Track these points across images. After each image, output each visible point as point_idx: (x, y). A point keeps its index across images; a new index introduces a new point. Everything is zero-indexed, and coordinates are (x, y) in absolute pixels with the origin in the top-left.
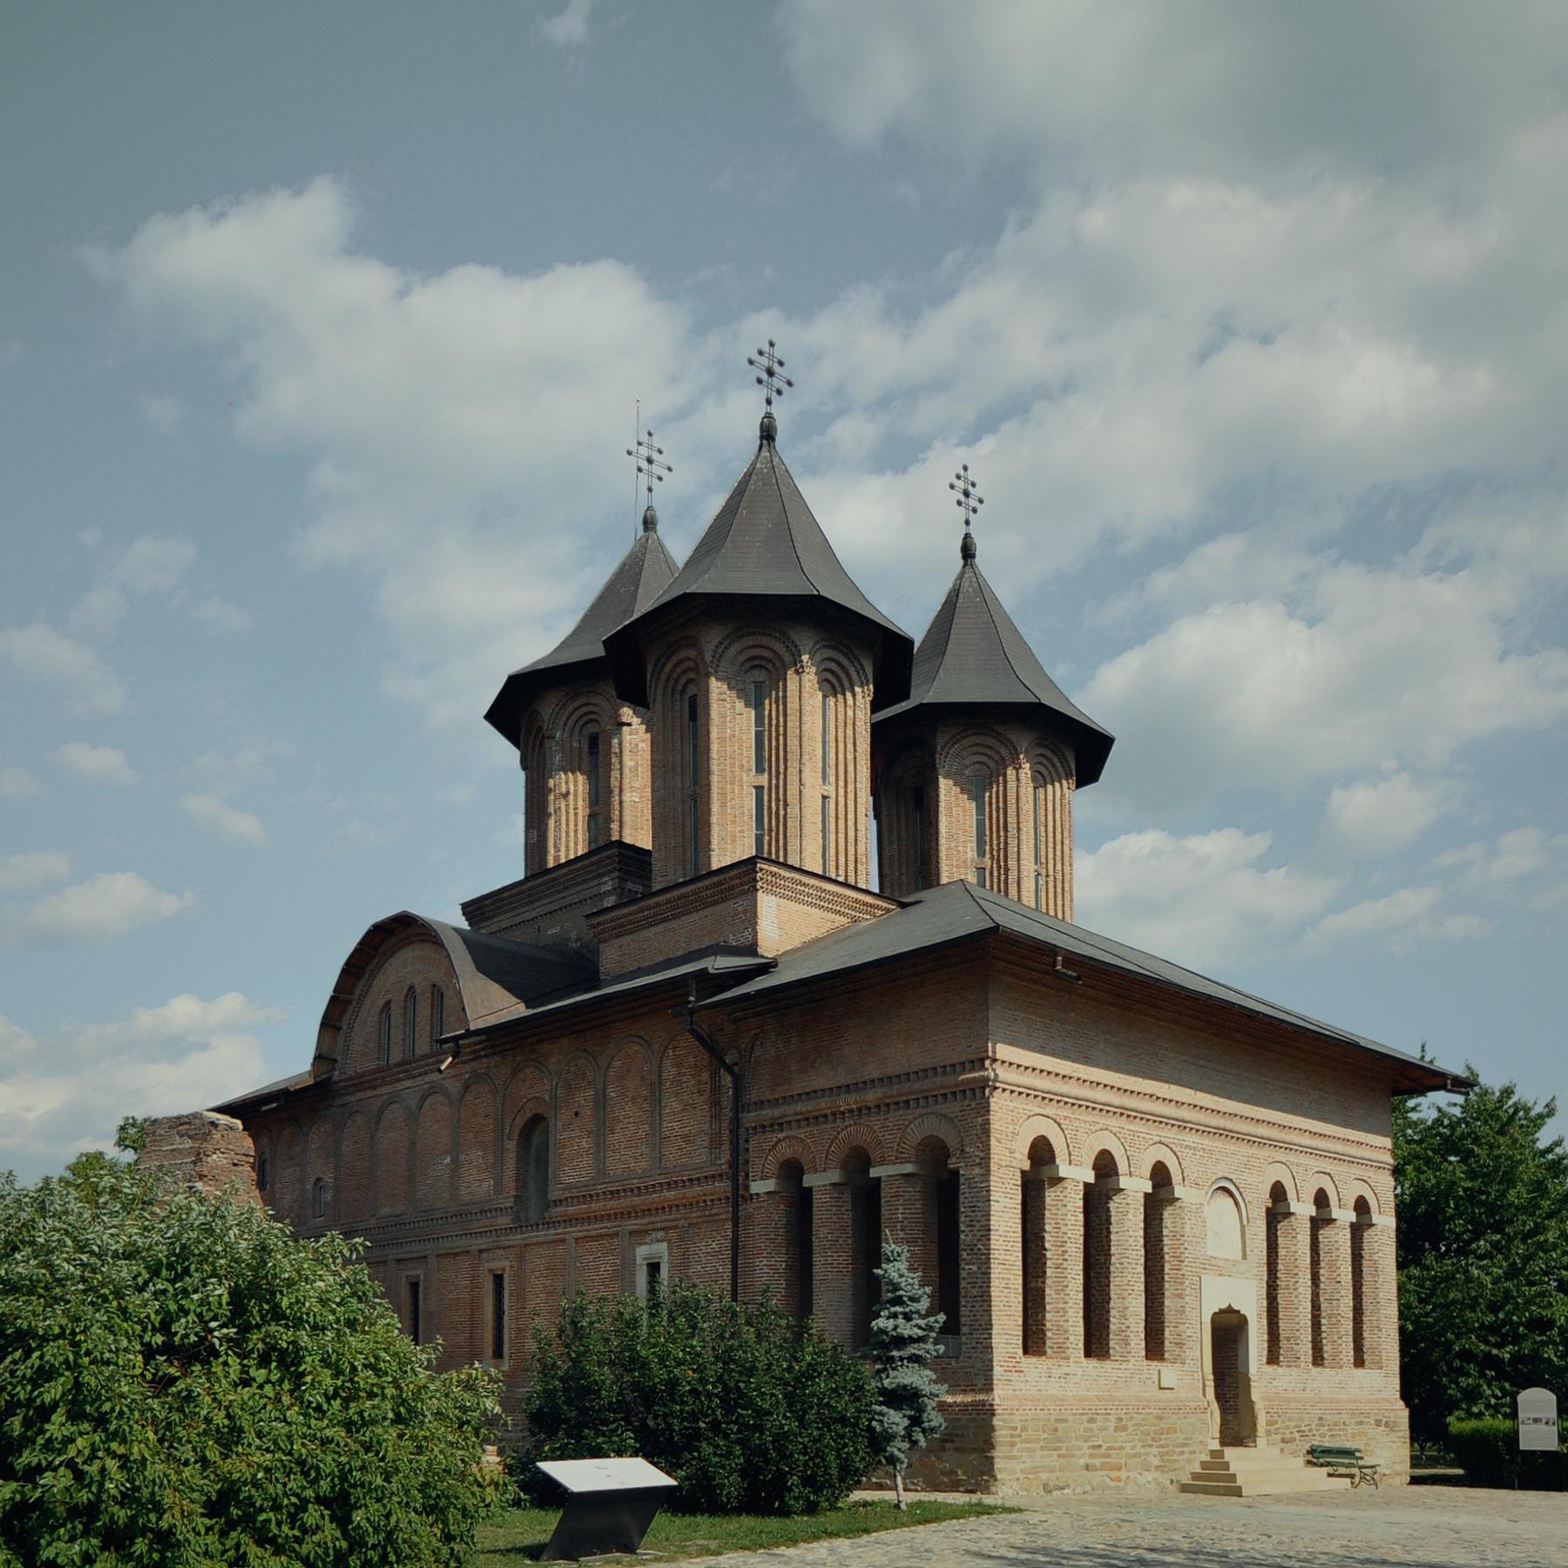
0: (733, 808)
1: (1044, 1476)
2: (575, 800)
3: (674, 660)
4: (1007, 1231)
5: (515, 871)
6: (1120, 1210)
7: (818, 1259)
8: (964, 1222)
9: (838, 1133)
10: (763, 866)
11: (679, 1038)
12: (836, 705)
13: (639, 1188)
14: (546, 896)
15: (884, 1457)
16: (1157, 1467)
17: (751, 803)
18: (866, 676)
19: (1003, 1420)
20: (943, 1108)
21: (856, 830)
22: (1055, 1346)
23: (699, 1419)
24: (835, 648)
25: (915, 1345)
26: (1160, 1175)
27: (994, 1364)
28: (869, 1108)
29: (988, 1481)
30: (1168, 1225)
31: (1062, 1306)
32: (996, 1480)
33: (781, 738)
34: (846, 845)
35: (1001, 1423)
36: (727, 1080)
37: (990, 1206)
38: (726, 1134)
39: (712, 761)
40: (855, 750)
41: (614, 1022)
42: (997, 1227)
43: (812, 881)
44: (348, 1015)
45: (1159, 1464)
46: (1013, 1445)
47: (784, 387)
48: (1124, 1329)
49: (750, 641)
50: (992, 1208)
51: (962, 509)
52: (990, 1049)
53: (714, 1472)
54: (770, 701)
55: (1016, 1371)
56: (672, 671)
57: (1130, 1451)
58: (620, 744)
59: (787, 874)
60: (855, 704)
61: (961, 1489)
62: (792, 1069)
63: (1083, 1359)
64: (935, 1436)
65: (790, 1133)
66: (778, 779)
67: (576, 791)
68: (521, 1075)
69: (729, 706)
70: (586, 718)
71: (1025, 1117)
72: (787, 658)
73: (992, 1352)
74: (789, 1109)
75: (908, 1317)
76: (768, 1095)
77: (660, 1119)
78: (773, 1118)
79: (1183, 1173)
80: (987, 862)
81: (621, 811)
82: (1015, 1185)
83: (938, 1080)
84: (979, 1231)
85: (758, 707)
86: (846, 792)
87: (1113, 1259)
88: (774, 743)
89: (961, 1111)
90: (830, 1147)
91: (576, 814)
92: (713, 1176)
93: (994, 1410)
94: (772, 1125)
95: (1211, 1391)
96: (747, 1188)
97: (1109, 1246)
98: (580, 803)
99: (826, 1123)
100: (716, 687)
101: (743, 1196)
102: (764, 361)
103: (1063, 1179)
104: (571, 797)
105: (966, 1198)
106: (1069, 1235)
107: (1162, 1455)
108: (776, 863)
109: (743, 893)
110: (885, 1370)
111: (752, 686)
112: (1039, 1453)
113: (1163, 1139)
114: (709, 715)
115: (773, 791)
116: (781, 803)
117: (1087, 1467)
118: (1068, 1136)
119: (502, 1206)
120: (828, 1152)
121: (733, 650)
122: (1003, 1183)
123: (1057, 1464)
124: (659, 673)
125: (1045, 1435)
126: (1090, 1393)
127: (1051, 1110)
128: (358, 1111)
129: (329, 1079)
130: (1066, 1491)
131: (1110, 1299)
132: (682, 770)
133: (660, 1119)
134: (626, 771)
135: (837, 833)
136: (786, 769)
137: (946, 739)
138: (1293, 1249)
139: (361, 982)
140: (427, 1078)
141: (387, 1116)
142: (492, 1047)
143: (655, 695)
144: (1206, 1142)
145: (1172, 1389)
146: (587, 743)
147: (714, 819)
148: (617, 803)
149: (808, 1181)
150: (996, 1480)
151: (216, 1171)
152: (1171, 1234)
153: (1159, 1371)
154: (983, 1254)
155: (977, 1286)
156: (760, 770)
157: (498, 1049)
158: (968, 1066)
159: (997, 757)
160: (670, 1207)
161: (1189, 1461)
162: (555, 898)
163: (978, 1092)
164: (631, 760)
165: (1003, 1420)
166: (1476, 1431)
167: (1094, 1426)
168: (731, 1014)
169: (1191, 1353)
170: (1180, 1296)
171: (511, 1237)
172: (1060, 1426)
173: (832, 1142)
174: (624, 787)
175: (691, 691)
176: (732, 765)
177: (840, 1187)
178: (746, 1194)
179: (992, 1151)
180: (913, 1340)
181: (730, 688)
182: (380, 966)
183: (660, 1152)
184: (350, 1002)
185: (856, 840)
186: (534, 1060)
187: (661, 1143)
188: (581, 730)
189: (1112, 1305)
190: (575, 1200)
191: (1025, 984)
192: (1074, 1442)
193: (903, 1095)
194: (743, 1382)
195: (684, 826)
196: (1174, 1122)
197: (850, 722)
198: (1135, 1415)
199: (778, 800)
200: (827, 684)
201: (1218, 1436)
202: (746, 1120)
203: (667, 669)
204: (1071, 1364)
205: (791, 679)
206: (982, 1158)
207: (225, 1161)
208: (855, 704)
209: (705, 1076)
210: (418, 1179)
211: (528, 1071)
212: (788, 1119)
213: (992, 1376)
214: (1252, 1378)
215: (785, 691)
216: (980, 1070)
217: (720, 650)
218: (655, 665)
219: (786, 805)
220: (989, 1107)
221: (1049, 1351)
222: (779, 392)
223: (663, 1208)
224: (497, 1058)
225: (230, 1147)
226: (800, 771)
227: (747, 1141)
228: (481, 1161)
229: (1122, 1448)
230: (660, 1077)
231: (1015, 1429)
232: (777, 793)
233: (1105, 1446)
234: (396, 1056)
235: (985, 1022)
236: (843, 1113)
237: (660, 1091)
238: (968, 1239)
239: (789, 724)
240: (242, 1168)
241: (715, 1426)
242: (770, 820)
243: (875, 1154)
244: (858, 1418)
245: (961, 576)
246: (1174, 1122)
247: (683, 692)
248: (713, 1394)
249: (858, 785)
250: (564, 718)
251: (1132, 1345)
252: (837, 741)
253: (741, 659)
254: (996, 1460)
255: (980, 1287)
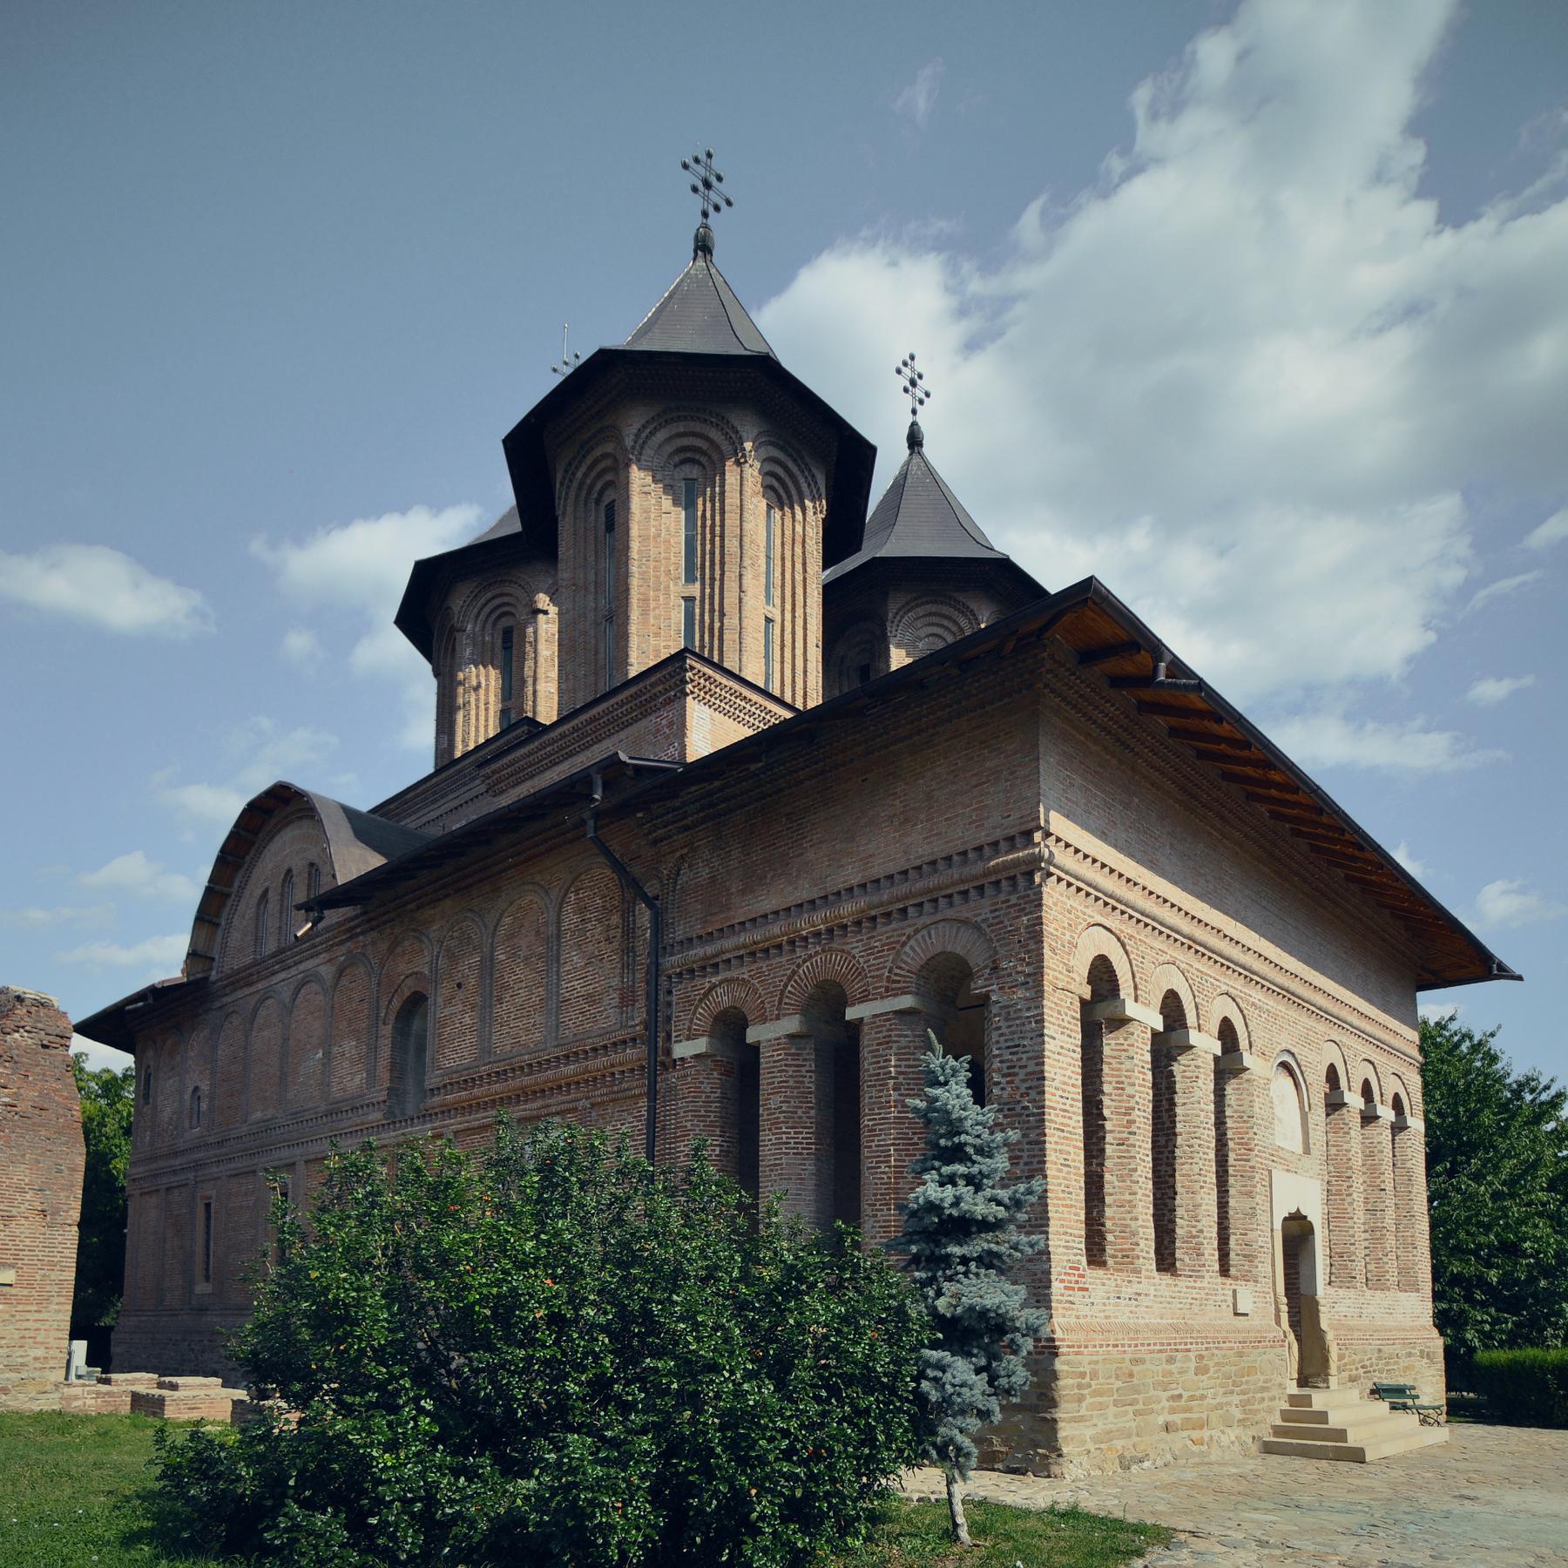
0: (657, 618)
1: (1119, 1444)
2: (487, 695)
3: (589, 460)
4: (1065, 1083)
5: (426, 766)
6: (1187, 1074)
7: (767, 1138)
8: (999, 1070)
9: (799, 966)
10: (694, 664)
11: (583, 877)
12: (783, 519)
13: (530, 1065)
14: (452, 791)
15: (934, 1445)
16: (1239, 1421)
17: (679, 616)
18: (818, 490)
19: (1068, 1363)
20: (961, 910)
21: (805, 660)
22: (1120, 1254)
23: (566, 1376)
24: (782, 449)
25: (990, 1236)
26: (1227, 1032)
27: (1053, 1277)
28: (845, 927)
29: (1047, 1457)
30: (1232, 1102)
31: (1128, 1197)
32: (1060, 1456)
33: (717, 539)
34: (794, 677)
35: (1065, 1368)
36: (644, 916)
37: (1043, 1043)
38: (641, 988)
39: (631, 562)
40: (805, 571)
41: (505, 870)
42: (1052, 1075)
43: (755, 697)
44: (227, 909)
45: (1241, 1417)
46: (1081, 1399)
47: (723, 205)
48: (1194, 1233)
49: (681, 427)
50: (1046, 1046)
51: (908, 397)
52: (1042, 816)
53: (591, 1502)
54: (705, 501)
55: (1080, 1289)
56: (585, 475)
57: (1212, 1401)
58: (535, 632)
59: (724, 681)
60: (804, 519)
61: (1000, 1466)
62: (734, 890)
63: (1155, 1274)
64: (1014, 1400)
65: (728, 975)
66: (712, 588)
67: (487, 685)
68: (399, 950)
69: (653, 501)
70: (498, 612)
71: (1085, 924)
72: (726, 447)
73: (1049, 1260)
74: (729, 943)
75: (975, 1182)
76: (698, 929)
77: (558, 979)
78: (706, 958)
79: (1249, 1037)
80: (695, 590)
81: (534, 702)
82: (1074, 1018)
83: (955, 873)
84: (1023, 1081)
85: (690, 506)
86: (794, 617)
87: (1179, 1140)
88: (708, 547)
89: (992, 912)
90: (786, 986)
91: (487, 709)
92: (624, 1042)
93: (1055, 1347)
94: (703, 968)
95: (1285, 1317)
96: (668, 1052)
97: (1174, 1122)
98: (492, 699)
99: (780, 955)
100: (639, 478)
101: (663, 1064)
102: (701, 170)
103: (1130, 1020)
104: (482, 692)
105: (1001, 1035)
106: (1137, 1099)
107: (1243, 1404)
108: (709, 662)
109: (669, 701)
110: (931, 1281)
111: (682, 484)
112: (1112, 1410)
113: (1231, 990)
114: (628, 508)
115: (707, 601)
116: (717, 613)
117: (1167, 1428)
118: (1134, 962)
119: (374, 1100)
120: (782, 992)
121: (661, 436)
122: (1059, 1013)
123: (1133, 1424)
124: (571, 481)
125: (1119, 1384)
126: (1164, 1321)
127: (1113, 921)
128: (234, 1012)
129: (206, 979)
130: (1146, 1464)
131: (1176, 1193)
132: (596, 587)
133: (558, 979)
134: (541, 660)
135: (782, 662)
136: (722, 575)
137: (898, 606)
138: (1346, 1146)
139: (242, 872)
140: (302, 967)
141: (262, 1012)
142: (369, 921)
143: (565, 506)
144: (1271, 1003)
145: (1246, 1315)
146: (500, 637)
147: (633, 629)
148: (530, 693)
149: (752, 1035)
150: (1060, 1456)
151: (16, 1052)
152: (1236, 1115)
153: (1234, 1292)
154: (1033, 1115)
155: (1022, 1161)
156: (690, 578)
157: (374, 923)
158: (1003, 846)
159: (954, 629)
160: (568, 1085)
161: (1270, 1411)
162: (462, 791)
163: (1021, 882)
164: (547, 649)
165: (1068, 1363)
166: (1514, 1361)
167: (1172, 1367)
168: (649, 833)
169: (1264, 1269)
170: (1250, 1195)
171: (383, 1136)
172: (1136, 1369)
173: (789, 979)
174: (538, 676)
175: (606, 500)
176: (656, 569)
177: (797, 1040)
178: (667, 1060)
179: (1045, 964)
180: (985, 1226)
181: (655, 481)
182: (260, 853)
183: (557, 1019)
184: (228, 896)
185: (805, 672)
186: (414, 930)
187: (558, 1008)
188: (494, 624)
189: (1178, 1201)
190: (456, 1086)
191: (1082, 738)
192: (1152, 1392)
193: (898, 900)
194: (659, 1302)
195: (597, 652)
196: (1241, 971)
197: (799, 539)
198: (1216, 1352)
199: (712, 611)
200: (772, 493)
201: (1296, 1376)
202: (668, 965)
203: (579, 475)
204: (1143, 1280)
205: (731, 471)
206: (1029, 975)
207: (30, 1041)
208: (804, 519)
209: (615, 919)
210: (290, 1079)
211: (407, 943)
212: (725, 957)
213: (1049, 1295)
214: (1321, 1301)
215: (722, 485)
216: (1025, 847)
217: (644, 435)
218: (566, 471)
219: (722, 614)
220: (1041, 899)
221: (1110, 1262)
222: (717, 208)
223: (560, 1087)
224: (374, 934)
225: (39, 1025)
226: (741, 575)
227: (670, 992)
228: (353, 1052)
229: (1203, 1397)
230: (559, 928)
231: (1083, 1375)
232: (712, 604)
233: (1186, 1395)
234: (271, 946)
235: (1033, 778)
236: (805, 939)
237: (559, 945)
238: (1005, 1094)
239: (727, 522)
240: (54, 1052)
241: (600, 1387)
242: (702, 637)
243: (852, 989)
244: (895, 1376)
245: (908, 463)
246: (1241, 971)
247: (598, 502)
248: (593, 1326)
249: (808, 611)
250: (476, 611)
251: (1206, 1256)
252: (783, 559)
253: (669, 448)
254: (1061, 1425)
255: (1026, 1164)
